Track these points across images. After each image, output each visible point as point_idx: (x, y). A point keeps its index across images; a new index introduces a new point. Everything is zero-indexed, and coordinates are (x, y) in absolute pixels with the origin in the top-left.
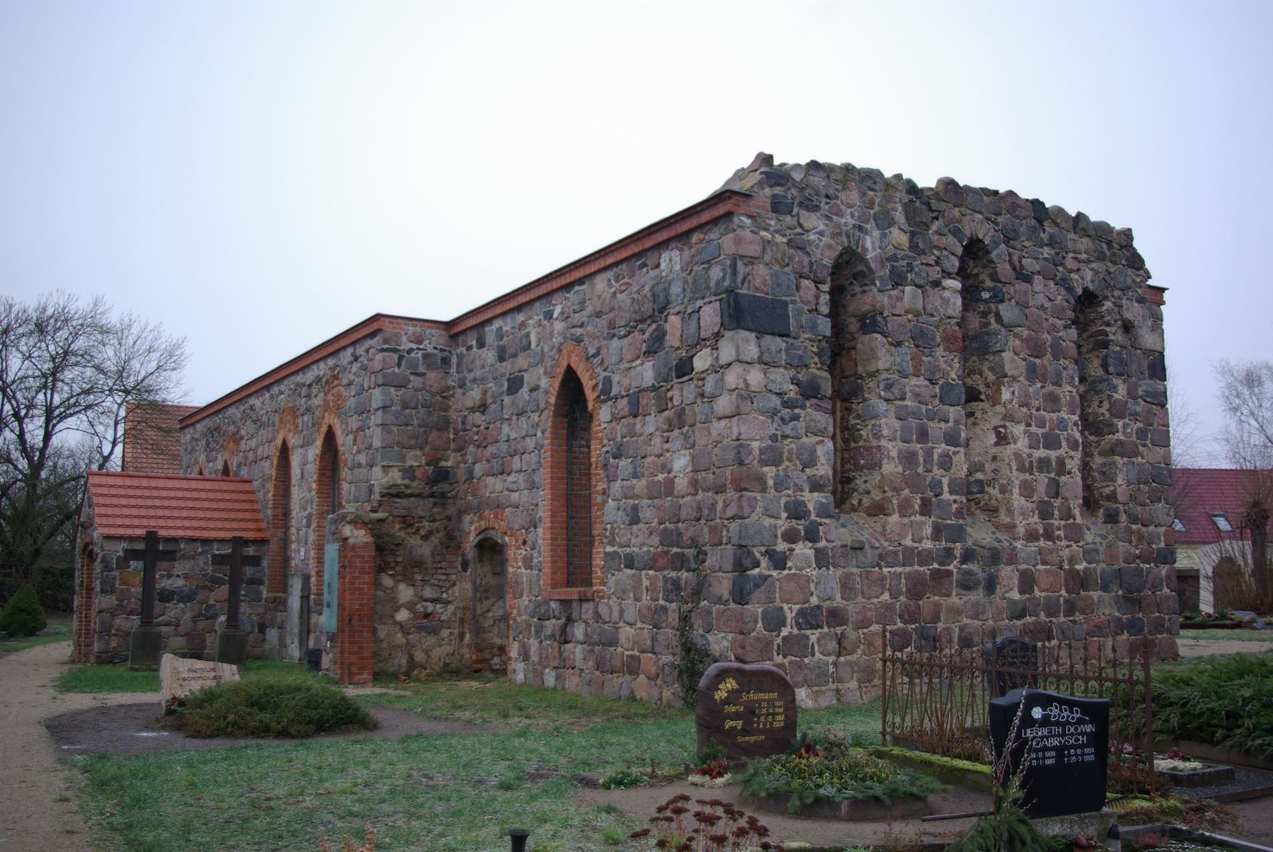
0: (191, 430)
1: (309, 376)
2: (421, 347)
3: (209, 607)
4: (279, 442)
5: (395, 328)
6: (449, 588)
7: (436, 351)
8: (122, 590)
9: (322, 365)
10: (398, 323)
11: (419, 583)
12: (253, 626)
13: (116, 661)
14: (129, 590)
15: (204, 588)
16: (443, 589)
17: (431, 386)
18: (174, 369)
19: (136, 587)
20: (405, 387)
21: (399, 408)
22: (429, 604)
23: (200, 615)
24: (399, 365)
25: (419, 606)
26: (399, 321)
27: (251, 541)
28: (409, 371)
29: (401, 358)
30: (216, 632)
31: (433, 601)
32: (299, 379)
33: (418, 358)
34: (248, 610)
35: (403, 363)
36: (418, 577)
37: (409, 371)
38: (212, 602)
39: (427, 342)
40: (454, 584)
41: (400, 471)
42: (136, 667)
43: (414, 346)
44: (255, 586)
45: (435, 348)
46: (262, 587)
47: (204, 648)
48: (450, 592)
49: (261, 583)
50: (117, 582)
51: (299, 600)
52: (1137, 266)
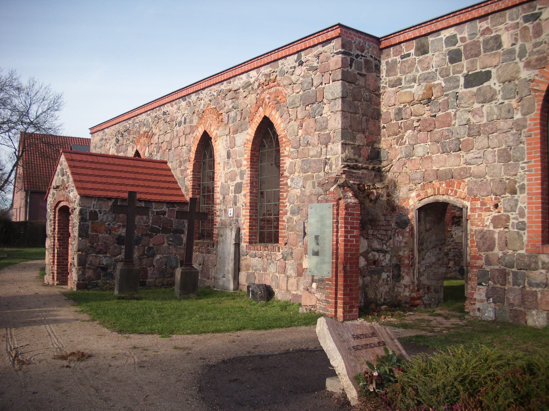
0: (101, 133)
1: (237, 83)
2: (363, 54)
3: (150, 249)
4: (199, 133)
5: (349, 37)
6: (387, 241)
7: (372, 59)
8: (93, 235)
9: (253, 73)
10: (350, 34)
11: (371, 237)
12: (177, 263)
13: (89, 287)
14: (97, 235)
15: (146, 235)
16: (384, 242)
17: (369, 85)
18: (56, 110)
19: (102, 233)
20: (354, 83)
21: (351, 99)
22: (376, 253)
23: (144, 254)
24: (351, 66)
25: (370, 255)
26: (351, 32)
27: (176, 203)
28: (357, 72)
29: (352, 61)
30: (154, 267)
31: (378, 251)
32: (224, 86)
33: (361, 62)
34: (174, 251)
35: (353, 65)
36: (370, 232)
37: (357, 72)
38: (151, 245)
39: (366, 51)
40: (390, 238)
41: (352, 148)
42: (123, 295)
43: (359, 53)
44: (178, 234)
45: (371, 57)
46: (182, 235)
47: (147, 278)
48: (388, 244)
49: (183, 232)
50: (90, 230)
51: (234, 246)
52: (489, 95)
